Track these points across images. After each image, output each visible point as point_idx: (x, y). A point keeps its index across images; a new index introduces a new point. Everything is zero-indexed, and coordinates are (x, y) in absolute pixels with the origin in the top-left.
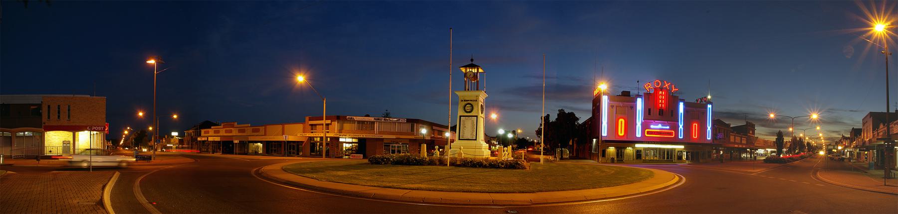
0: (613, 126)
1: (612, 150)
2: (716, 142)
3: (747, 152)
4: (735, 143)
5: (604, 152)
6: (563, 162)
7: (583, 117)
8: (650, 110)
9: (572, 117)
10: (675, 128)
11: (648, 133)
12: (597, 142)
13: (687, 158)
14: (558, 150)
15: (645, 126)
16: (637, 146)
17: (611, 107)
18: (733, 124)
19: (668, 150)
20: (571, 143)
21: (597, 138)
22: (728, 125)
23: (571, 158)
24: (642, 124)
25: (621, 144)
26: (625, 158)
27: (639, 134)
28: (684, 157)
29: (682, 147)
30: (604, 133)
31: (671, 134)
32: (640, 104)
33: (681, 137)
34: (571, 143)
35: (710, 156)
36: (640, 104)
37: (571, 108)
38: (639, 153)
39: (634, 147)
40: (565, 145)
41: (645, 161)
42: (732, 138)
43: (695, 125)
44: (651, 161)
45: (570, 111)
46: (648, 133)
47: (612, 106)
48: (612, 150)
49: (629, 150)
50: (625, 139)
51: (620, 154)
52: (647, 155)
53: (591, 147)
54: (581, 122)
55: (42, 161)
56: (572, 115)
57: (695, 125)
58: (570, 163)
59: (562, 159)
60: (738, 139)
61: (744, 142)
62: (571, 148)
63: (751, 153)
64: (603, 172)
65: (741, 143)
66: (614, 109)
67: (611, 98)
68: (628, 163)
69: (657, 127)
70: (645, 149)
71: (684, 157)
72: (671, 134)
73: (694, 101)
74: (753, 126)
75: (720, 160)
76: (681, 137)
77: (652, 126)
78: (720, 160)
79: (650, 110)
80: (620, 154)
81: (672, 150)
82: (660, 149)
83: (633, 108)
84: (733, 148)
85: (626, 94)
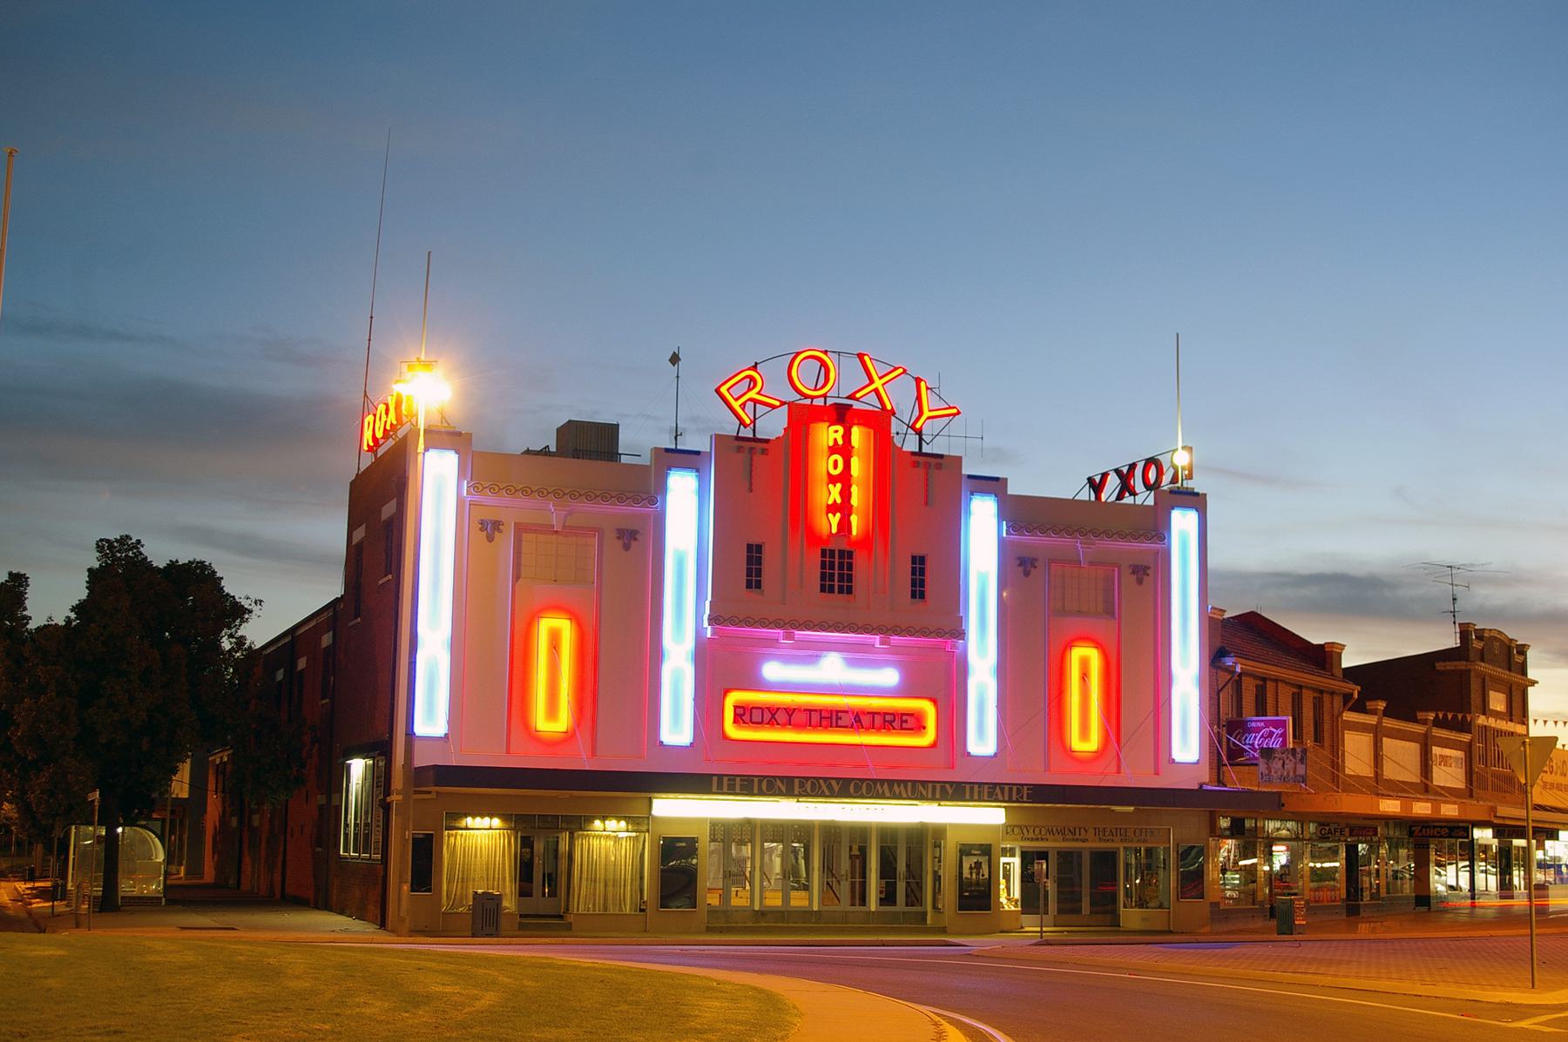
0: (494, 668)
1: (482, 838)
2: (1237, 780)
3: (1470, 852)
4: (1379, 785)
5: (425, 854)
6: (114, 936)
7: (278, 599)
8: (754, 555)
9: (195, 597)
10: (949, 692)
11: (744, 715)
12: (380, 781)
13: (1031, 899)
14: (84, 837)
15: (720, 668)
16: (670, 808)
17: (479, 529)
18: (1361, 648)
19: (889, 837)
20: (180, 786)
21: (379, 749)
22: (1323, 657)
23: (178, 898)
24: (705, 656)
25: (551, 799)
26: (583, 899)
27: (677, 726)
28: (1009, 894)
29: (992, 815)
30: (431, 713)
31: (912, 723)
32: (685, 508)
33: (982, 740)
34: (180, 786)
35: (1193, 881)
36: (685, 508)
37: (206, 536)
38: (676, 867)
39: (641, 821)
40: (134, 800)
41: (724, 923)
42: (1356, 751)
43: (1085, 659)
44: (765, 921)
45: (185, 554)
46: (744, 715)
47: (491, 528)
48: (482, 838)
49: (609, 841)
50: (580, 760)
51: (542, 872)
52: (734, 875)
53: (331, 814)
54: (259, 631)
55: (854, 501)
56: (195, 580)
57: (1085, 659)
58: (169, 943)
59: (109, 904)
60: (1401, 758)
61: (1448, 774)
62: (179, 825)
63: (1504, 861)
64: (417, 1000)
65: (1425, 788)
66: (507, 540)
67: (484, 468)
68: (606, 926)
69: (830, 671)
70: (726, 833)
71: (1009, 894)
72: (912, 723)
73: (1072, 488)
74: (1512, 659)
75: (1274, 912)
76: (982, 740)
77: (772, 671)
78: (1274, 912)
79: (754, 555)
80: (542, 872)
81: (922, 839)
82: (831, 833)
83: (640, 540)
84: (1366, 827)
85: (590, 442)
